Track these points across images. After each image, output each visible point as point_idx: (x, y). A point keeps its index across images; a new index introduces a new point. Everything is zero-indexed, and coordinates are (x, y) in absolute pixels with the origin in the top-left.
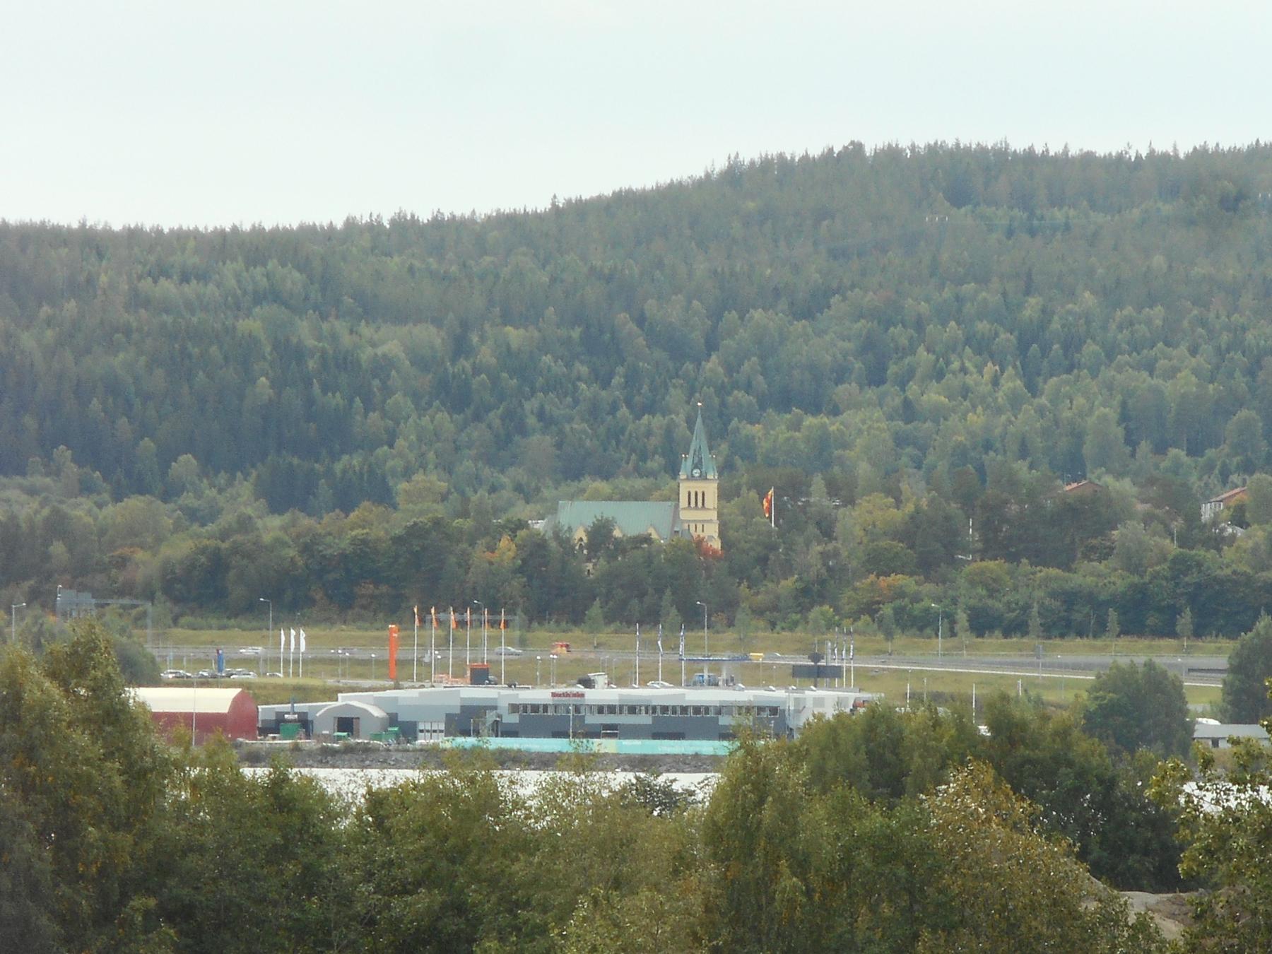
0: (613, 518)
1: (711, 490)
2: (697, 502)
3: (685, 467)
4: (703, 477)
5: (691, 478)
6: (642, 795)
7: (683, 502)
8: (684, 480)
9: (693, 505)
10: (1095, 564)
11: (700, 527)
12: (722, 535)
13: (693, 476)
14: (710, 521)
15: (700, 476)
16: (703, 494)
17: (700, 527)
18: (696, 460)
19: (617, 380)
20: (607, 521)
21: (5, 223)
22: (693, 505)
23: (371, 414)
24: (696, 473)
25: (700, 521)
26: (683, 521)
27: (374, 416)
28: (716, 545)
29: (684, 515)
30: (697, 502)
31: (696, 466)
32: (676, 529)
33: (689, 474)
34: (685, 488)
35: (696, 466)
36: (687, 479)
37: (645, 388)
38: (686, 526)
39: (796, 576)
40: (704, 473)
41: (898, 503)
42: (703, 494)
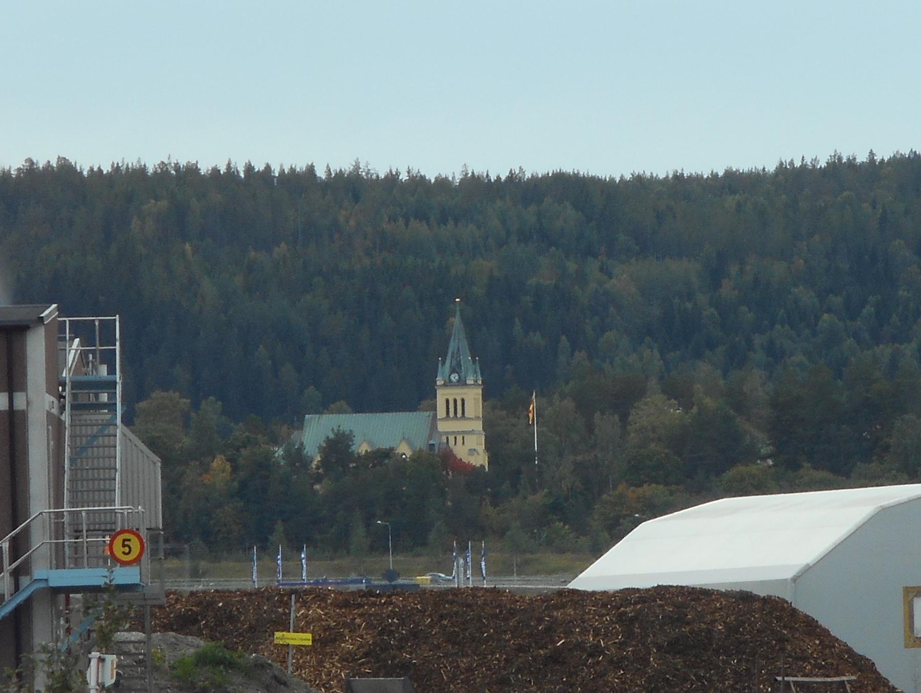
0: (351, 431)
1: (473, 397)
2: (457, 410)
3: (443, 373)
4: (462, 383)
5: (448, 384)
6: (512, 636)
7: (441, 412)
8: (441, 386)
9: (452, 414)
10: (515, 502)
11: (459, 439)
12: (490, 446)
13: (450, 381)
14: (472, 432)
15: (458, 381)
16: (463, 400)
17: (459, 439)
18: (454, 362)
19: (868, 310)
20: (343, 434)
21: (6, 175)
22: (452, 414)
23: (577, 353)
24: (454, 377)
25: (458, 433)
26: (441, 434)
27: (580, 355)
28: (480, 459)
29: (442, 427)
30: (457, 410)
31: (453, 371)
32: (431, 442)
33: (447, 380)
34: (442, 395)
35: (453, 371)
36: (445, 385)
37: (895, 318)
38: (444, 439)
39: (546, 490)
40: (463, 378)
41: (687, 407)
42: (463, 400)
